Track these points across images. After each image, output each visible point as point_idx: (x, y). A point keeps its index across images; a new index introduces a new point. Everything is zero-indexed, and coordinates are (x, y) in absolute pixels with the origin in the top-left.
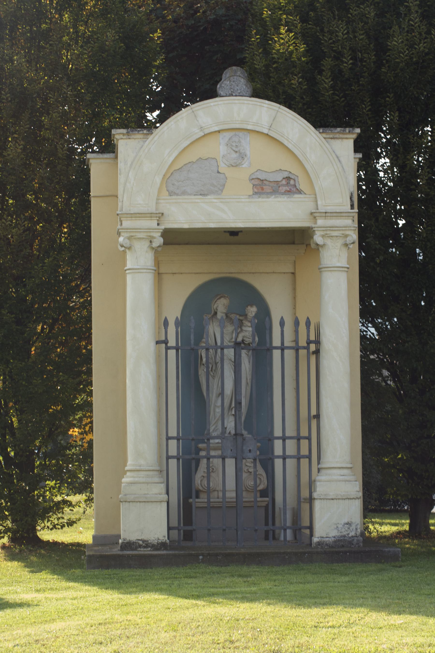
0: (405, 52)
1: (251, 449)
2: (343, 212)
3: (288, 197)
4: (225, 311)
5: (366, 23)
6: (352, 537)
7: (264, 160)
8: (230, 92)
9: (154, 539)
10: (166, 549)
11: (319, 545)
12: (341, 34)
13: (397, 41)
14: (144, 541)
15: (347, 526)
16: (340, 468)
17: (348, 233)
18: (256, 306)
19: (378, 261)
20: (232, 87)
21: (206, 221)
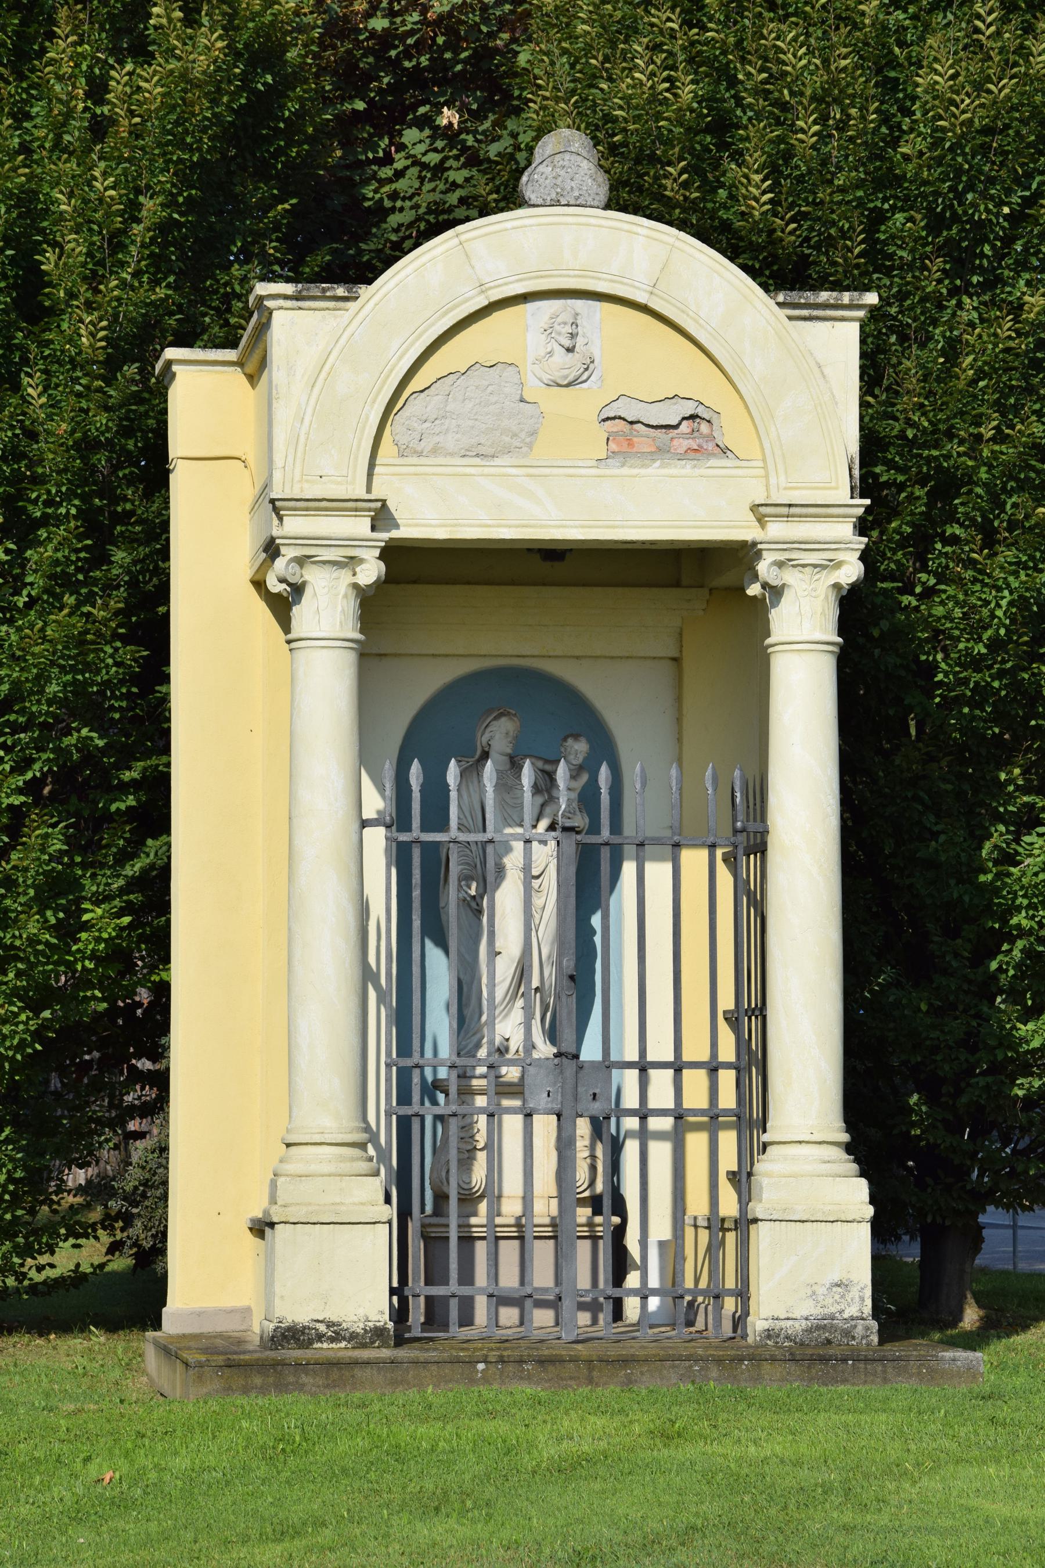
0: (963, 101)
1: (597, 1091)
2: (796, 505)
3: (695, 466)
4: (509, 751)
5: (855, 27)
6: (852, 1318)
7: (641, 369)
8: (554, 196)
9: (355, 1319)
10: (384, 1345)
11: (769, 1337)
12: (790, 56)
13: (935, 78)
14: (330, 1324)
15: (839, 1290)
16: (820, 1143)
17: (840, 556)
18: (589, 741)
19: (876, 633)
20: (559, 181)
21: (490, 522)
